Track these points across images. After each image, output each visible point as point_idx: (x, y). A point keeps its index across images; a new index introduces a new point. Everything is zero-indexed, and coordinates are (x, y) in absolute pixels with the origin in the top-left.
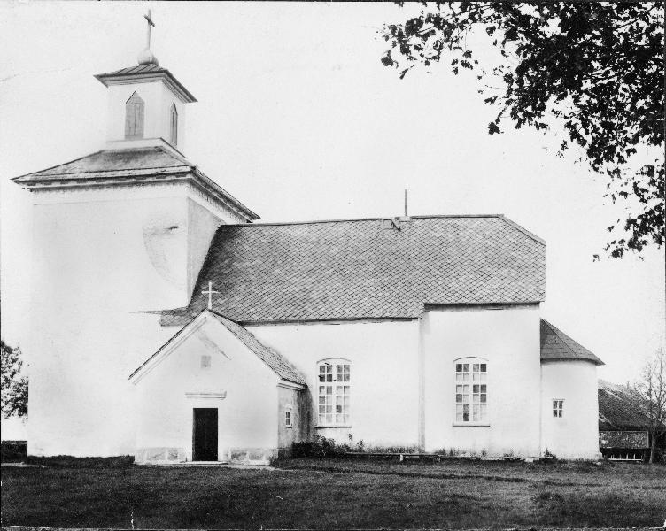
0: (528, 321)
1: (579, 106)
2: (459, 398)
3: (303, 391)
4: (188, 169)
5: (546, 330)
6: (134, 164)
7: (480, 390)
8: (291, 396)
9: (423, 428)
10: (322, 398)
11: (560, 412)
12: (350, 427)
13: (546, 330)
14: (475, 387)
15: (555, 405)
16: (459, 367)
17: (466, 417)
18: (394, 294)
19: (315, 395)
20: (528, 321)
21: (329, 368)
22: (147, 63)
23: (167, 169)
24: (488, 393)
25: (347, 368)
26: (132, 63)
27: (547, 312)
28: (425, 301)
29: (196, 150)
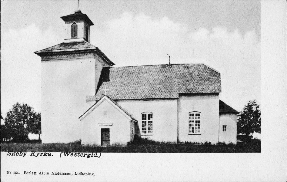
0: (214, 102)
1: (257, 109)
2: (190, 125)
3: (136, 123)
4: (95, 48)
5: (222, 104)
6: (75, 46)
7: (198, 123)
8: (133, 124)
9: (178, 134)
10: (143, 126)
11: (225, 129)
12: (153, 135)
13: (222, 104)
14: (196, 122)
15: (223, 128)
16: (190, 115)
17: (193, 132)
18: (168, 90)
19: (140, 125)
20: (214, 102)
21: (146, 115)
22: (78, 12)
23: (88, 48)
24: (201, 123)
25: (152, 115)
26: (72, 12)
27: (222, 97)
28: (179, 92)
29: (95, 42)
